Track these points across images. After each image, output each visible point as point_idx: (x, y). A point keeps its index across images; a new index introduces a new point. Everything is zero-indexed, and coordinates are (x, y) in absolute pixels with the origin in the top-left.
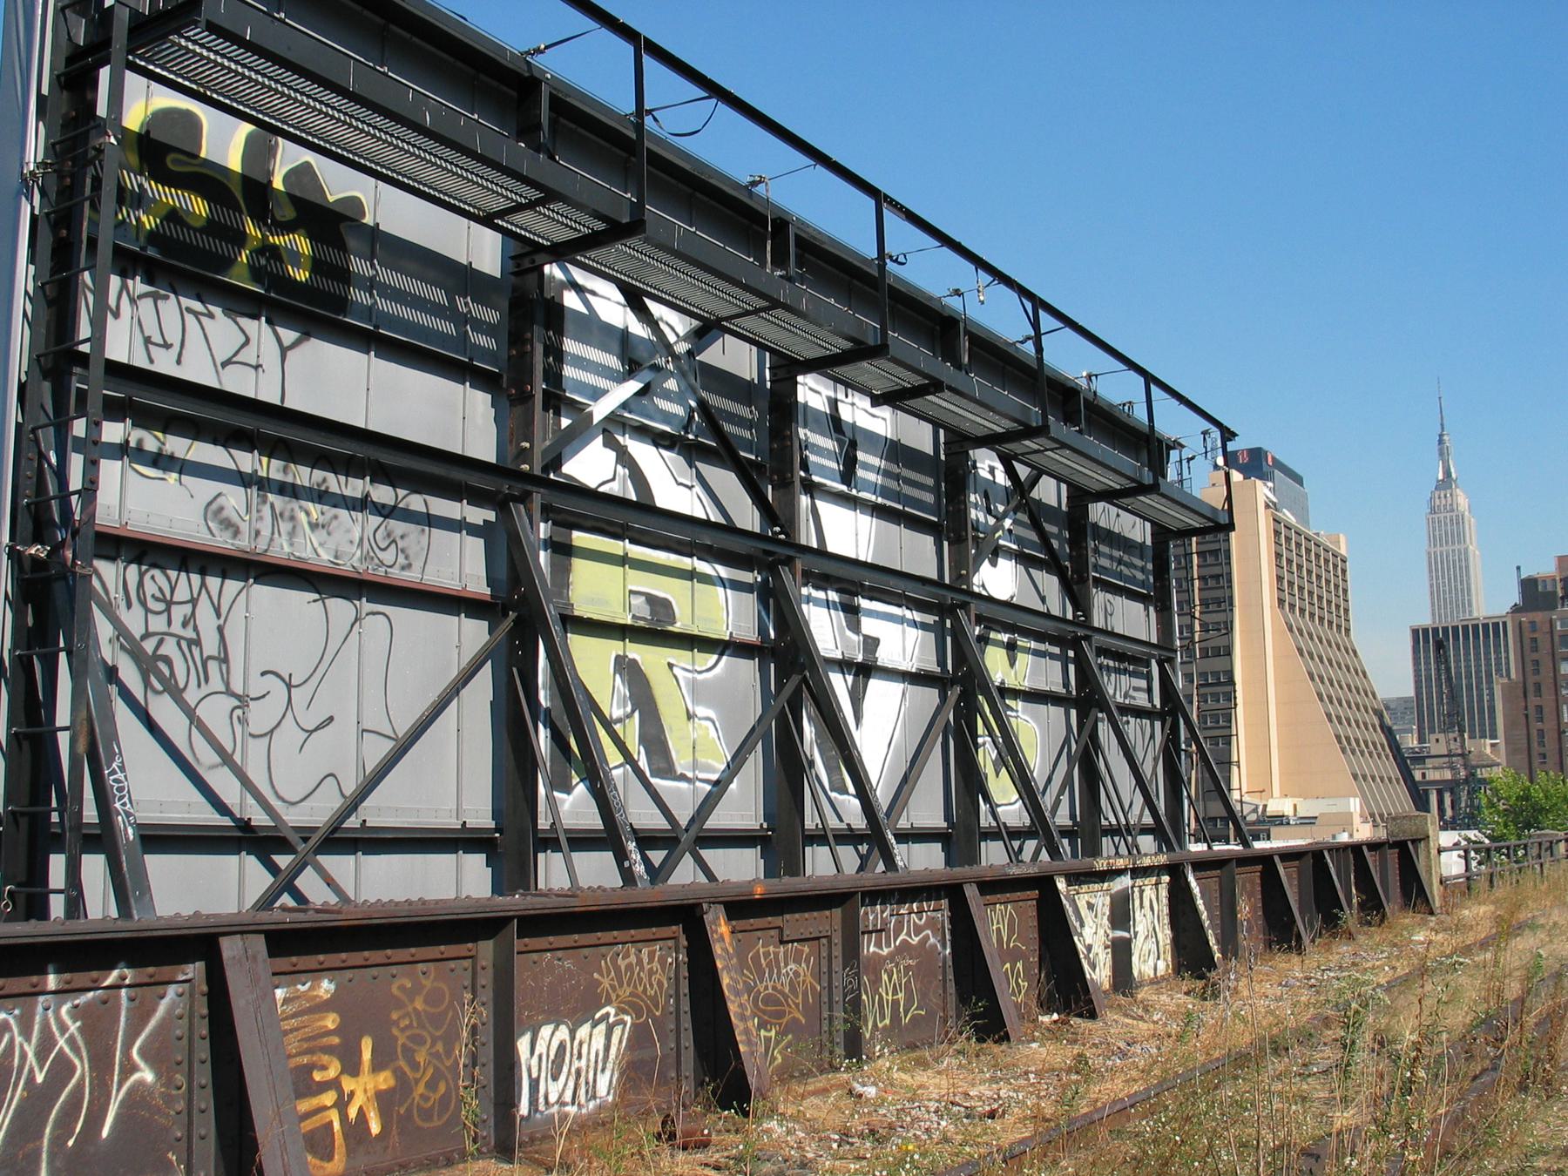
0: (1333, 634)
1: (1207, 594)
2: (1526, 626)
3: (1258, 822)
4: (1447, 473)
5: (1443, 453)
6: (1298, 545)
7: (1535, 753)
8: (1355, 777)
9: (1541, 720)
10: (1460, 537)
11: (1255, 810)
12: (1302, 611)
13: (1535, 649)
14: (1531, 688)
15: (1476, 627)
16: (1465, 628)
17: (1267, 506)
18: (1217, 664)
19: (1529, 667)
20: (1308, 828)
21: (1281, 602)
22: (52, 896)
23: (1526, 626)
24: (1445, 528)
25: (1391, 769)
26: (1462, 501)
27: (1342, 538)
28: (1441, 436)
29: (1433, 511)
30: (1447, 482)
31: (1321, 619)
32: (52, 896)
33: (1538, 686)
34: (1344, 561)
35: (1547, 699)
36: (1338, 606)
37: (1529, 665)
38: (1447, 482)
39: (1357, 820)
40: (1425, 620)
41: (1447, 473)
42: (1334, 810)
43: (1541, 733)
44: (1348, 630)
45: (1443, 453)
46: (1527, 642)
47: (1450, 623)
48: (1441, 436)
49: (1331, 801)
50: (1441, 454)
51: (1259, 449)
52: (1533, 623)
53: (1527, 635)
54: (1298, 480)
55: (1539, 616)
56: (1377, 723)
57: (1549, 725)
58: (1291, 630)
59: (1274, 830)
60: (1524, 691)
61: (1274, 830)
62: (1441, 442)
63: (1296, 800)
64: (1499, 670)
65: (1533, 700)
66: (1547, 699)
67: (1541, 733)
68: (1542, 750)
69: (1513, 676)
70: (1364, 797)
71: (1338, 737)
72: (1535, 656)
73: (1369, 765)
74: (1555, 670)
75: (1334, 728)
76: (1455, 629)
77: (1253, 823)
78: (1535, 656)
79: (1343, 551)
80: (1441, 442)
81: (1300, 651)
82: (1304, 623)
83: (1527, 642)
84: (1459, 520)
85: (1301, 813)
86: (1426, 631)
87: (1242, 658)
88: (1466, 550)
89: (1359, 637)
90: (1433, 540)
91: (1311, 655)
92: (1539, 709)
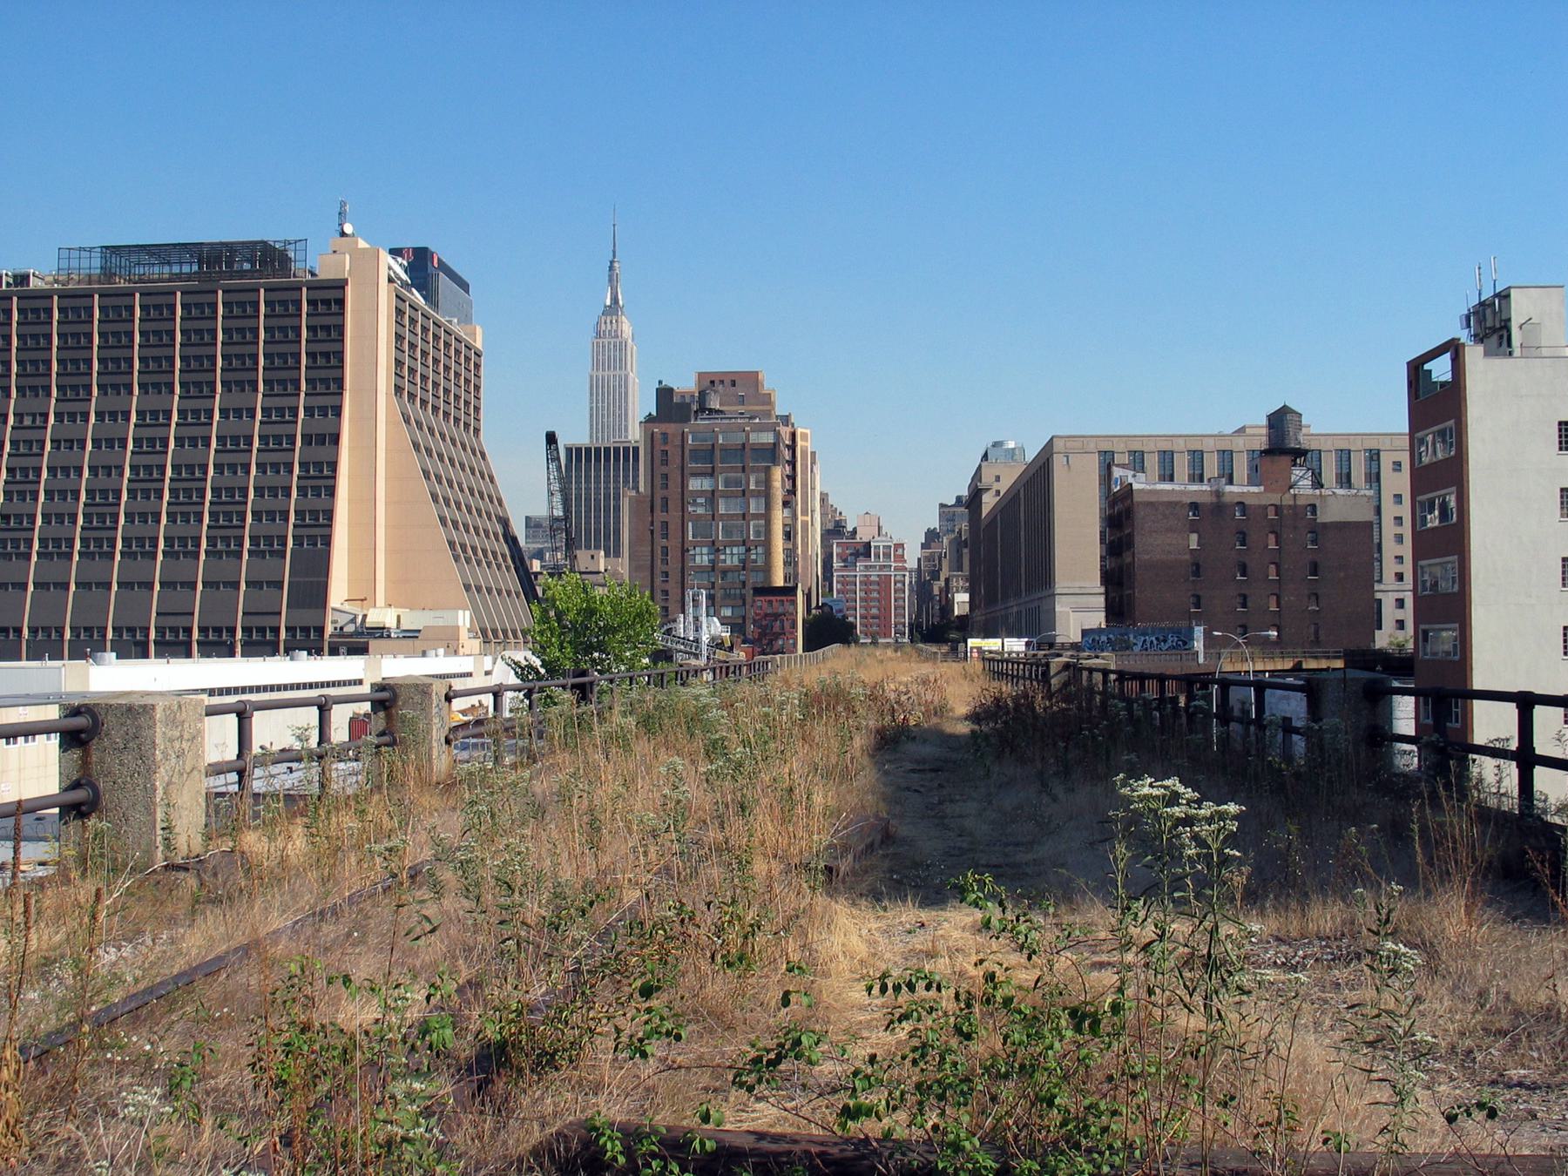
0: (459, 433)
1: (315, 374)
2: (658, 437)
3: (357, 634)
4: (615, 300)
5: (612, 280)
6: (458, 352)
7: (657, 571)
8: (467, 588)
9: (666, 536)
10: (622, 363)
11: (353, 621)
12: (457, 420)
13: (665, 462)
14: (658, 503)
15: (626, 449)
16: (617, 450)
17: (390, 280)
18: (321, 453)
19: (658, 481)
20: (410, 641)
21: (399, 389)
22: (1478, 706)
23: (658, 437)
24: (609, 352)
25: (512, 581)
26: (627, 328)
27: (479, 330)
28: (612, 262)
29: (598, 335)
30: (613, 308)
31: (467, 425)
32: (1478, 706)
33: (665, 501)
34: (478, 355)
35: (674, 516)
36: (467, 403)
37: (659, 479)
38: (613, 308)
39: (464, 635)
40: (576, 434)
41: (615, 300)
42: (441, 623)
43: (665, 551)
44: (477, 431)
45: (612, 280)
46: (658, 454)
47: (610, 443)
48: (612, 262)
49: (438, 613)
50: (610, 280)
51: (425, 250)
52: (665, 435)
53: (659, 447)
54: (464, 286)
55: (671, 428)
56: (500, 530)
57: (673, 543)
58: (407, 421)
59: (373, 644)
60: (651, 505)
61: (373, 644)
62: (611, 268)
63: (400, 611)
64: (626, 482)
65: (660, 516)
66: (674, 516)
67: (665, 551)
68: (665, 568)
69: (642, 489)
70: (476, 610)
71: (451, 544)
72: (664, 469)
73: (484, 576)
74: (683, 485)
75: (448, 533)
76: (607, 450)
77: (351, 635)
78: (664, 469)
79: (479, 345)
80: (611, 268)
81: (416, 446)
82: (427, 416)
83: (658, 454)
84: (621, 347)
85: (404, 626)
86: (579, 450)
87: (351, 449)
88: (626, 377)
89: (488, 439)
90: (597, 364)
91: (462, 466)
92: (665, 525)
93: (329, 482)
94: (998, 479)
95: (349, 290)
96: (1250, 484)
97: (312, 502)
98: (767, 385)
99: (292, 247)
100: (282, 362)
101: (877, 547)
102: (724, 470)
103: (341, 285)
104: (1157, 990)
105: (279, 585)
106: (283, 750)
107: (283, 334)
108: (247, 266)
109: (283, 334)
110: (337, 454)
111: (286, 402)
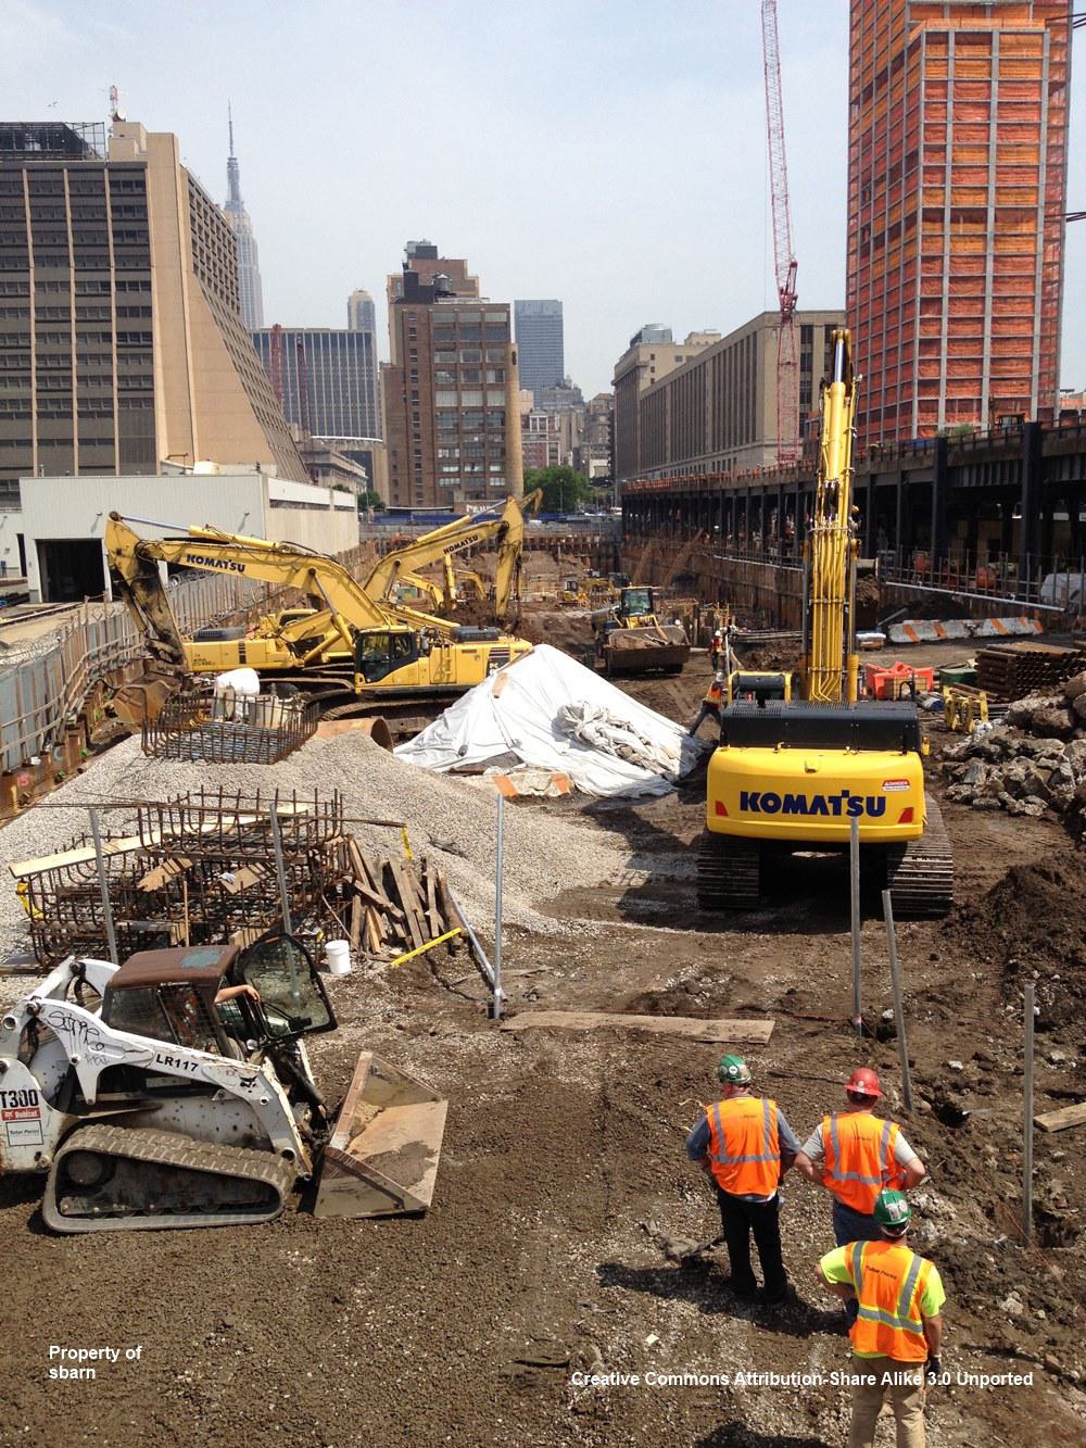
74: (431, 359)
93: (147, 351)
94: (653, 357)
95: (148, 172)
96: (44, 601)
97: (133, 369)
98: (471, 272)
99: (90, 129)
100: (90, 241)
101: (534, 420)
102: (466, 346)
103: (140, 168)
104: (473, 1269)
105: (111, 442)
106: (826, 370)
107: (89, 215)
108: (37, 147)
109: (89, 215)
110: (151, 325)
111: (99, 277)
